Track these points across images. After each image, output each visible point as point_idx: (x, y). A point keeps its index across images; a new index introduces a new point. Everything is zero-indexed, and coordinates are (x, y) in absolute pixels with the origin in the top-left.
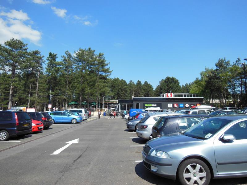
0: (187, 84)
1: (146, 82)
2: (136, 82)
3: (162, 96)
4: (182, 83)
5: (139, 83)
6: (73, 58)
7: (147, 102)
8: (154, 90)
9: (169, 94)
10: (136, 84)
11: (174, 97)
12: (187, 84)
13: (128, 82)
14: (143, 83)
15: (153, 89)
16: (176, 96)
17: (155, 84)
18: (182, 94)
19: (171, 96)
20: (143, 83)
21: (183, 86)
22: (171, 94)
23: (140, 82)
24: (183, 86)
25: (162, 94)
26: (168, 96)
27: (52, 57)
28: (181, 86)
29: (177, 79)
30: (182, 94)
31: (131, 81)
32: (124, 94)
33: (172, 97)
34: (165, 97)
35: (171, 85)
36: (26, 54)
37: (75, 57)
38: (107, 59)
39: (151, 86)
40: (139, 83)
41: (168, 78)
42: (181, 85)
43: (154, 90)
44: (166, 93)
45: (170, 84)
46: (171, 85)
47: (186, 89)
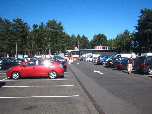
0: (112, 39)
1: (83, 36)
2: (76, 36)
3: (95, 48)
4: (108, 38)
5: (79, 36)
6: (44, 26)
7: (87, 52)
8: (89, 42)
9: (99, 47)
10: (76, 37)
11: (102, 49)
12: (112, 39)
13: (71, 36)
14: (81, 36)
15: (88, 41)
16: (103, 48)
17: (90, 38)
18: (106, 47)
19: (101, 48)
20: (81, 36)
21: (109, 40)
22: (101, 47)
23: (80, 36)
24: (109, 40)
25: (95, 47)
26: (99, 48)
27: (35, 26)
28: (108, 40)
29: (97, 34)
30: (106, 47)
31: (73, 35)
32: (18, 27)
33: (99, 49)
34: (97, 49)
35: (101, 40)
36: (145, 21)
37: (45, 25)
38: (64, 25)
39: (88, 39)
40: (79, 36)
41: (99, 35)
42: (108, 39)
43: (89, 42)
44: (98, 47)
45: (100, 39)
46: (101, 40)
47: (110, 43)
